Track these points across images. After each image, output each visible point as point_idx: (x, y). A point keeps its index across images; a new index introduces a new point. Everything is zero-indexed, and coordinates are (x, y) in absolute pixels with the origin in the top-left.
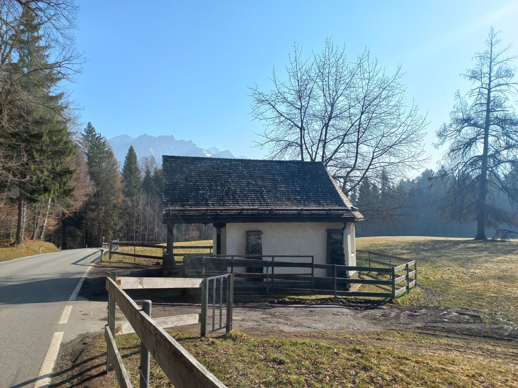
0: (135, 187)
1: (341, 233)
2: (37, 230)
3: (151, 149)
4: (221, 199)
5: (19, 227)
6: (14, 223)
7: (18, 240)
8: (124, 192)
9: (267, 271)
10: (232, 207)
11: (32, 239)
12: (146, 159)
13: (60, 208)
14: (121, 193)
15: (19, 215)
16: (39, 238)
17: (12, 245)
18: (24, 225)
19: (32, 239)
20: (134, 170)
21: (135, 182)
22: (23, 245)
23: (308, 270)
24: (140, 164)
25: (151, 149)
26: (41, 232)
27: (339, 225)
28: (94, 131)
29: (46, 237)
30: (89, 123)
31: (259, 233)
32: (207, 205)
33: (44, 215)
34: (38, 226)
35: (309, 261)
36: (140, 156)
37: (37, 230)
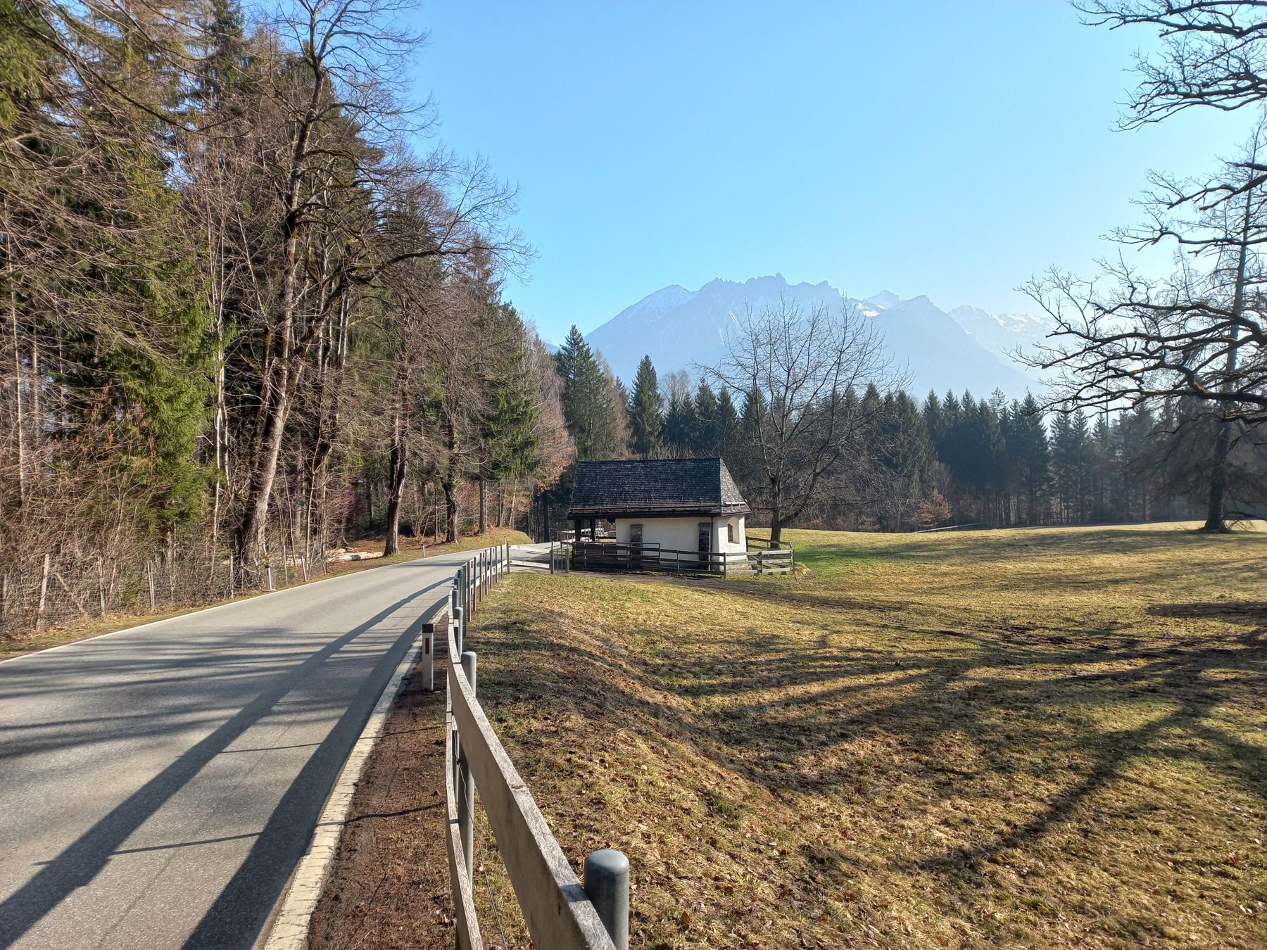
0: (651, 433)
1: (711, 525)
2: (504, 514)
3: (731, 313)
4: (615, 499)
5: (482, 513)
6: (476, 507)
7: (482, 530)
8: (629, 446)
9: (645, 553)
10: (621, 506)
11: (498, 526)
12: (673, 377)
13: (531, 481)
14: (624, 446)
15: (482, 498)
16: (506, 524)
17: (476, 534)
18: (486, 511)
19: (498, 526)
20: (647, 404)
21: (651, 425)
22: (486, 534)
23: (656, 553)
24: (663, 389)
25: (731, 313)
26: (509, 517)
27: (708, 520)
28: (581, 340)
29: (516, 523)
30: (574, 328)
31: (640, 527)
32: (602, 505)
33: (510, 494)
34: (505, 508)
35: (657, 547)
36: (660, 371)
37: (504, 514)
